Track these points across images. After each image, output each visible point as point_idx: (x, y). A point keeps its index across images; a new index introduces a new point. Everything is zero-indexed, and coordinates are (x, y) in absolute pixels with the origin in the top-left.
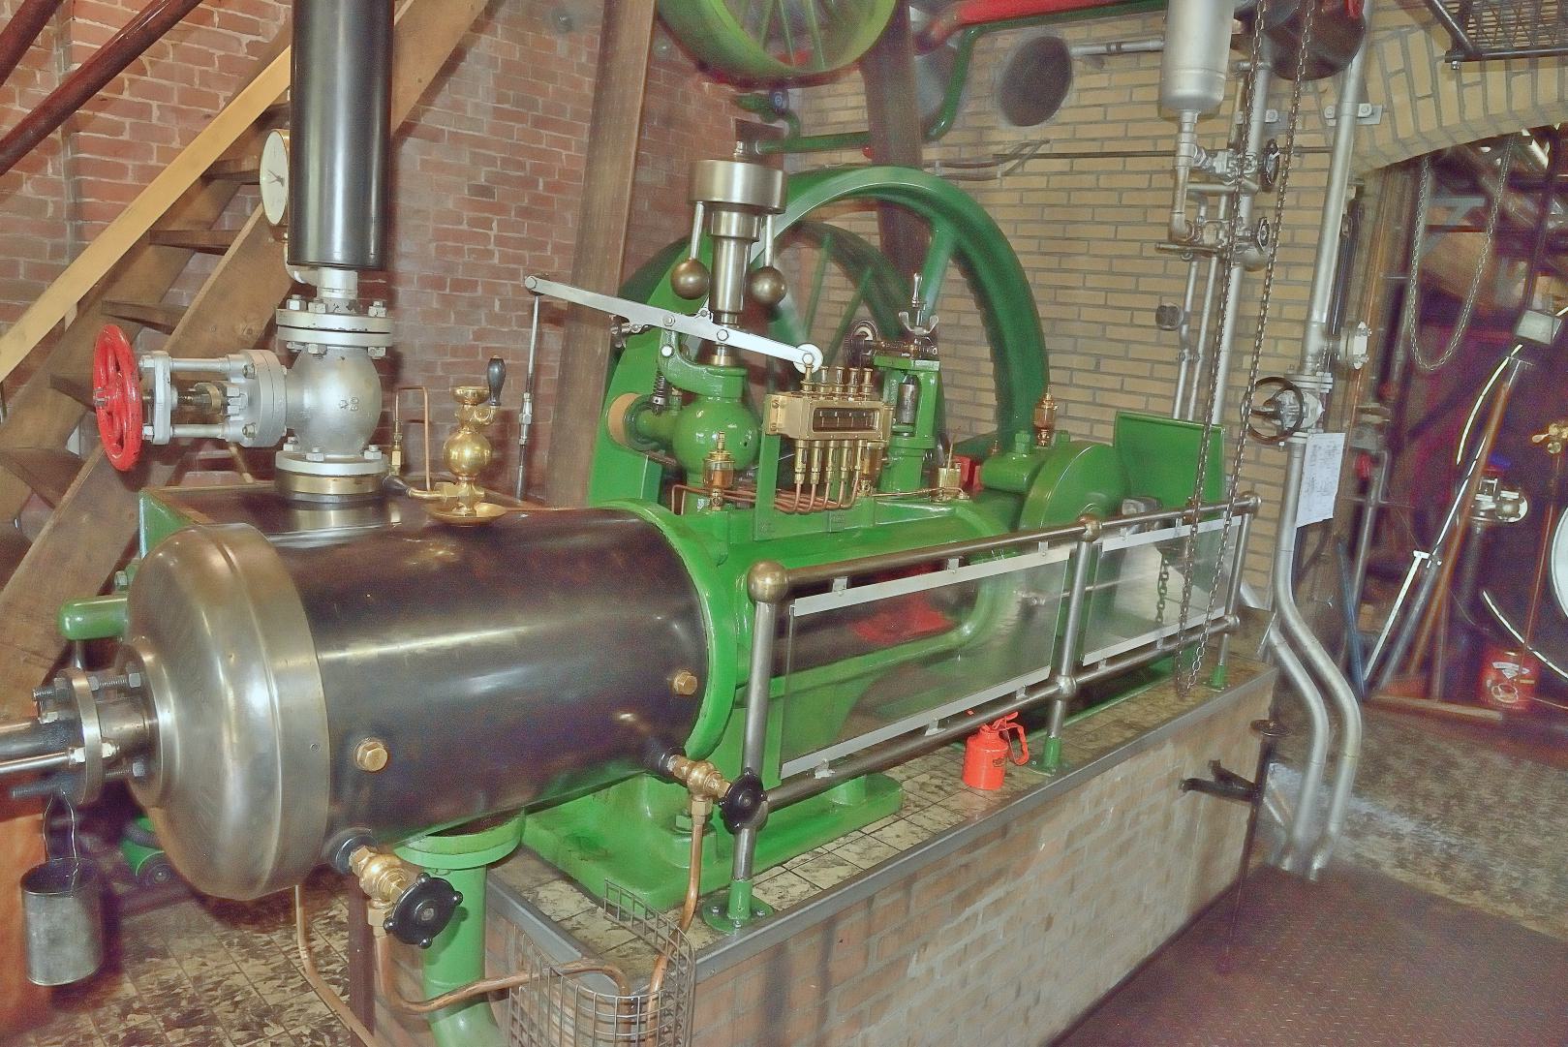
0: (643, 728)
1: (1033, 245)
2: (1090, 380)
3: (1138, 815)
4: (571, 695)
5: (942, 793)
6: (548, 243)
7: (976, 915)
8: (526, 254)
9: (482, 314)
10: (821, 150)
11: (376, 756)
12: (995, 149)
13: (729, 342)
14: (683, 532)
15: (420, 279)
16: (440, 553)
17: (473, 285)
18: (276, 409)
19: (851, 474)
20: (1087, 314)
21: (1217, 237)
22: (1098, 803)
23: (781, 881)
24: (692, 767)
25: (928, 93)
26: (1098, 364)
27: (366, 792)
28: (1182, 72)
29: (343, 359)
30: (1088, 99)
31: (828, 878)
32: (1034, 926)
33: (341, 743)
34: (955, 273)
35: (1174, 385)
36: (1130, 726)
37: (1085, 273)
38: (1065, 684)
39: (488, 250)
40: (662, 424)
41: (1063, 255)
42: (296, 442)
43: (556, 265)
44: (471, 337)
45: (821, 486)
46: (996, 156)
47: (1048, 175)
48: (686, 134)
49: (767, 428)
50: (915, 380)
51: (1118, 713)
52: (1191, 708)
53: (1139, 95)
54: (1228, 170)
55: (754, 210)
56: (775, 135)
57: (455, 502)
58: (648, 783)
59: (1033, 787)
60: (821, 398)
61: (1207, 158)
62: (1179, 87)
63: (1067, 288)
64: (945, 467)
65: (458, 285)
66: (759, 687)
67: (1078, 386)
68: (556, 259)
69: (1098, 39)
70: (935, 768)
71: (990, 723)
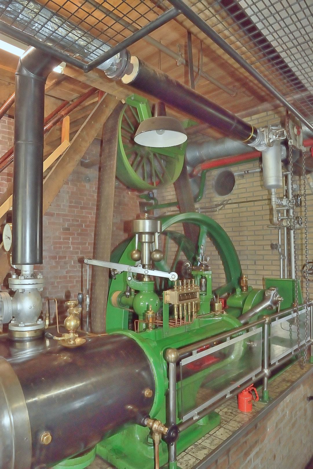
0: (136, 410)
1: (230, 229)
2: (254, 267)
3: (296, 412)
4: (110, 402)
5: (233, 415)
6: (86, 243)
7: (251, 460)
8: (80, 246)
9: (68, 266)
10: (163, 208)
11: (47, 439)
12: (215, 203)
13: (149, 274)
14: (143, 340)
15: (49, 257)
16: (65, 358)
17: (65, 257)
19: (192, 312)
20: (249, 248)
21: (287, 223)
22: (283, 410)
23: (186, 458)
24: (153, 423)
25: (194, 189)
26: (255, 262)
27: (44, 452)
28: (270, 178)
29: (30, 293)
30: (240, 187)
31: (201, 455)
32: (270, 459)
33: (35, 435)
34: (209, 240)
35: (279, 267)
36: (288, 381)
37: (247, 236)
38: (266, 371)
39: (69, 246)
40: (129, 301)
41: (240, 231)
42: (15, 320)
43: (90, 249)
44: (65, 273)
45: (183, 318)
46: (216, 205)
47: (232, 209)
48: (125, 207)
49: (164, 301)
50: (205, 278)
51: (283, 376)
52: (306, 372)
53: (255, 184)
54: (287, 204)
55: (152, 234)
56: (151, 205)
57: (69, 340)
58: (137, 427)
59: (263, 409)
60: (180, 291)
61: (280, 201)
62: (269, 183)
63: (242, 241)
64: (217, 303)
65: (60, 258)
66: (173, 392)
67: (250, 270)
68: (89, 247)
69: (241, 170)
70: (228, 405)
71: (245, 389)
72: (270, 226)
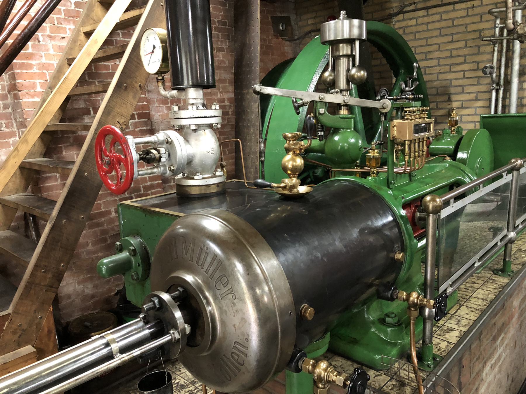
18: (184, 157)
72: (485, 39)
